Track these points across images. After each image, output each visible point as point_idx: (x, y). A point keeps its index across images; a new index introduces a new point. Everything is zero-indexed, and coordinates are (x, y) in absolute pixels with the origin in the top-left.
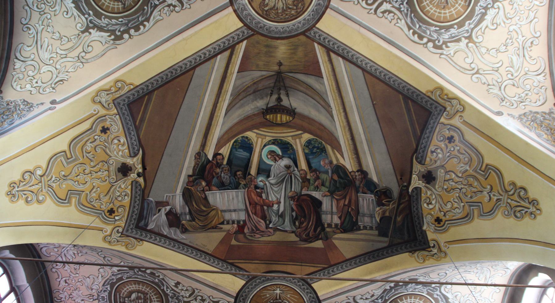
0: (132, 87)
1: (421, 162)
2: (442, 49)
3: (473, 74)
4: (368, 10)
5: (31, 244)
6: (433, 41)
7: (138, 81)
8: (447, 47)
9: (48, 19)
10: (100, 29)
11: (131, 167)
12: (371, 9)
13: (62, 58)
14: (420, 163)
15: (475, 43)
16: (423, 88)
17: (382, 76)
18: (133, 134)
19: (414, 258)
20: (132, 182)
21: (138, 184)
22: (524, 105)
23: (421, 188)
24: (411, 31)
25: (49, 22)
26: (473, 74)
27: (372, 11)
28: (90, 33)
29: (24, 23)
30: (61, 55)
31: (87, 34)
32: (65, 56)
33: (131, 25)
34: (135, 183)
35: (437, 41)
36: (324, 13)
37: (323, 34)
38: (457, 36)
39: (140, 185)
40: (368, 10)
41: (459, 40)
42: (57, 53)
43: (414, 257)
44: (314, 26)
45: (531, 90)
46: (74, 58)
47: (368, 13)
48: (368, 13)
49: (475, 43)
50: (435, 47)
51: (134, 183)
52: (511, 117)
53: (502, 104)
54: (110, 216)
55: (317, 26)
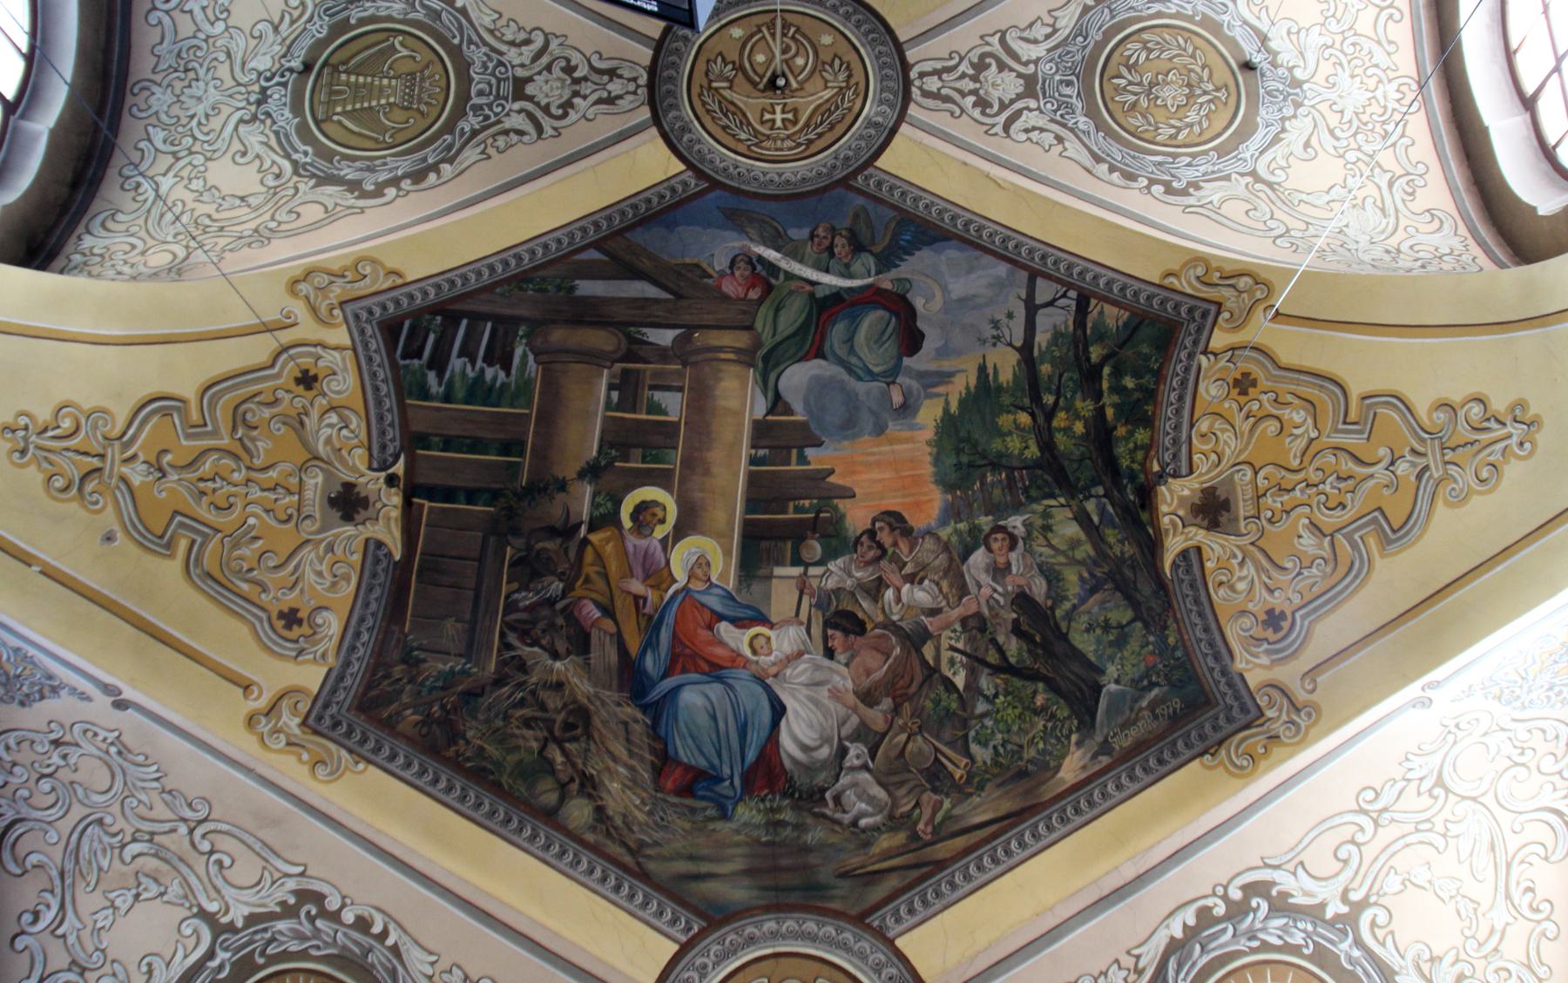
0: (399, 281)
1: (374, 548)
2: (297, 893)
3: (206, 820)
4: (987, 127)
5: (1518, 264)
6: (324, 913)
7: (417, 268)
8: (283, 904)
9: (1473, 937)
10: (1314, 913)
11: (366, 499)
12: (993, 126)
13: (1428, 820)
14: (380, 544)
15: (203, 914)
16: (1151, 272)
17: (487, 802)
18: (388, 405)
19: (1221, 769)
20: (367, 540)
21: (381, 553)
22: (52, 732)
23: (370, 468)
24: (390, 942)
25: (1470, 928)
26: (206, 820)
27: (998, 129)
28: (1344, 898)
29: (1546, 924)
30: (1430, 830)
31: (1355, 896)
32: (1421, 827)
33: (1224, 930)
34: (374, 548)
35: (314, 912)
36: (893, 132)
37: (887, 178)
38: (256, 932)
39: (389, 555)
40: (987, 127)
41: (251, 920)
42: (1444, 836)
43: (1221, 763)
44: (684, 949)
45: (35, 776)
46: (1393, 820)
47: (986, 132)
48: (986, 132)
49: (203, 914)
50: (319, 898)
51: (372, 547)
52: (83, 693)
53: (116, 734)
54: (285, 633)
55: (675, 948)
